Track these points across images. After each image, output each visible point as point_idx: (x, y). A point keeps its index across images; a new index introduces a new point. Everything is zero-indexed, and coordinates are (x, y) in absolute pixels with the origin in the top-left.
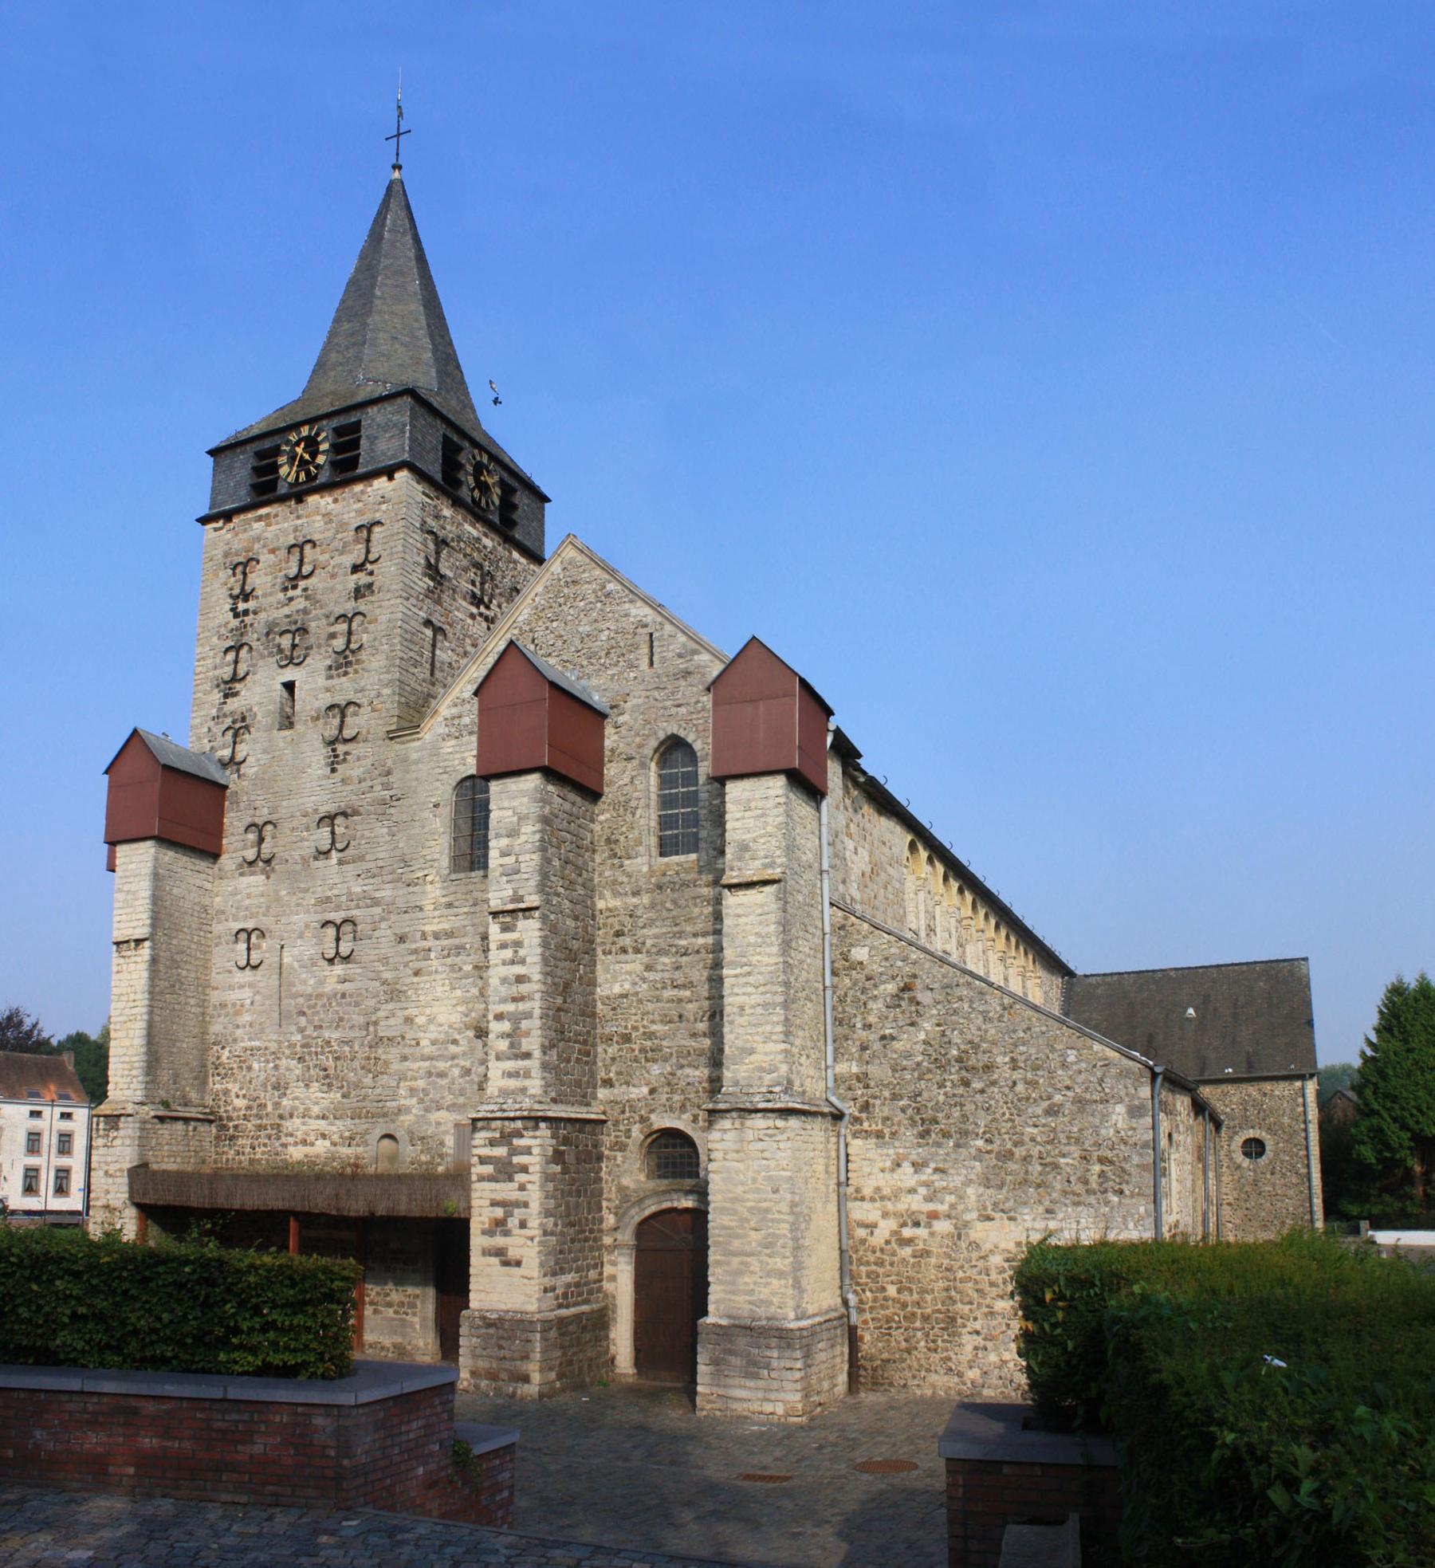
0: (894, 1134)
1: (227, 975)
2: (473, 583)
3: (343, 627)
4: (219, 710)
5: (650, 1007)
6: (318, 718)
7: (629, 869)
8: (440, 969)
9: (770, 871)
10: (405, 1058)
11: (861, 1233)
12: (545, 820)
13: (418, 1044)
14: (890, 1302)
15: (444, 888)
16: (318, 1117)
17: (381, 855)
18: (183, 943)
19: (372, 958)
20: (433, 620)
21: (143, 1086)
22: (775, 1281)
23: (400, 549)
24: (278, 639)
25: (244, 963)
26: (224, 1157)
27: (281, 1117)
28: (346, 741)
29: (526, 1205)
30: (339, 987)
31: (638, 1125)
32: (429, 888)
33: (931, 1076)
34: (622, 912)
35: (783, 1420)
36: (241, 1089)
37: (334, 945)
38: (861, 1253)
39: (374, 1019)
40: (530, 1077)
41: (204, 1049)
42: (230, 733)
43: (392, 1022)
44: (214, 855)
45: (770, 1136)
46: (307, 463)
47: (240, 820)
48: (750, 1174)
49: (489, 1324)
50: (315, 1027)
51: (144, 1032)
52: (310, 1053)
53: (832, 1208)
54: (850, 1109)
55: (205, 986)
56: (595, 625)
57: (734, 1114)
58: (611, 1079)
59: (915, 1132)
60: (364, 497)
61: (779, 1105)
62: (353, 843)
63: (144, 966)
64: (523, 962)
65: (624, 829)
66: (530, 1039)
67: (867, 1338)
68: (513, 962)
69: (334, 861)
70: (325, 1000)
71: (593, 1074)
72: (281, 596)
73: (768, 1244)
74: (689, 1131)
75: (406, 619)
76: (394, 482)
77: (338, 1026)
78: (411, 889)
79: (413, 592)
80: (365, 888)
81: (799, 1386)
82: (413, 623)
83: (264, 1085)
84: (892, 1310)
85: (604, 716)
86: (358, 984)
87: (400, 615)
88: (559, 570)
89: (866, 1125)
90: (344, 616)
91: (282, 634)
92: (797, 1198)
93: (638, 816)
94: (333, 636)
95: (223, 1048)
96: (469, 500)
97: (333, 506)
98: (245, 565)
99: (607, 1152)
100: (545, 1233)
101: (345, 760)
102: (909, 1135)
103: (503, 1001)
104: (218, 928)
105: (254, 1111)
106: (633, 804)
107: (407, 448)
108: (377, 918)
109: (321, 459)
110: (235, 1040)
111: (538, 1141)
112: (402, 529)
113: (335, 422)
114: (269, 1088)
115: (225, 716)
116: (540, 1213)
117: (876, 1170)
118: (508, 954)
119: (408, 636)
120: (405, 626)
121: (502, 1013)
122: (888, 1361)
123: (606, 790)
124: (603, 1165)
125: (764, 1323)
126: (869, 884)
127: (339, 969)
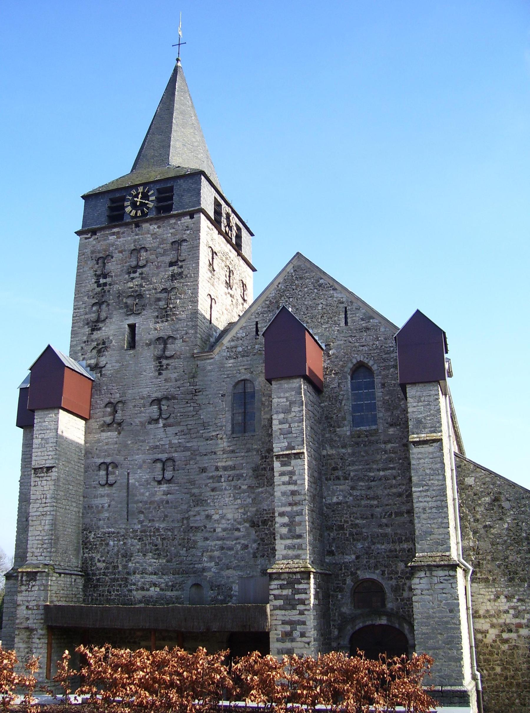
5: (355, 509)
10: (206, 539)
16: (151, 574)
27: (128, 573)
29: (304, 623)
30: (164, 497)
36: (101, 557)
39: (187, 516)
50: (149, 520)
52: (146, 536)
62: (172, 415)
68: (289, 483)
69: (161, 425)
80: (180, 441)
95: (90, 532)
98: (104, 258)
114: (120, 556)
115: (92, 341)
118: (286, 478)
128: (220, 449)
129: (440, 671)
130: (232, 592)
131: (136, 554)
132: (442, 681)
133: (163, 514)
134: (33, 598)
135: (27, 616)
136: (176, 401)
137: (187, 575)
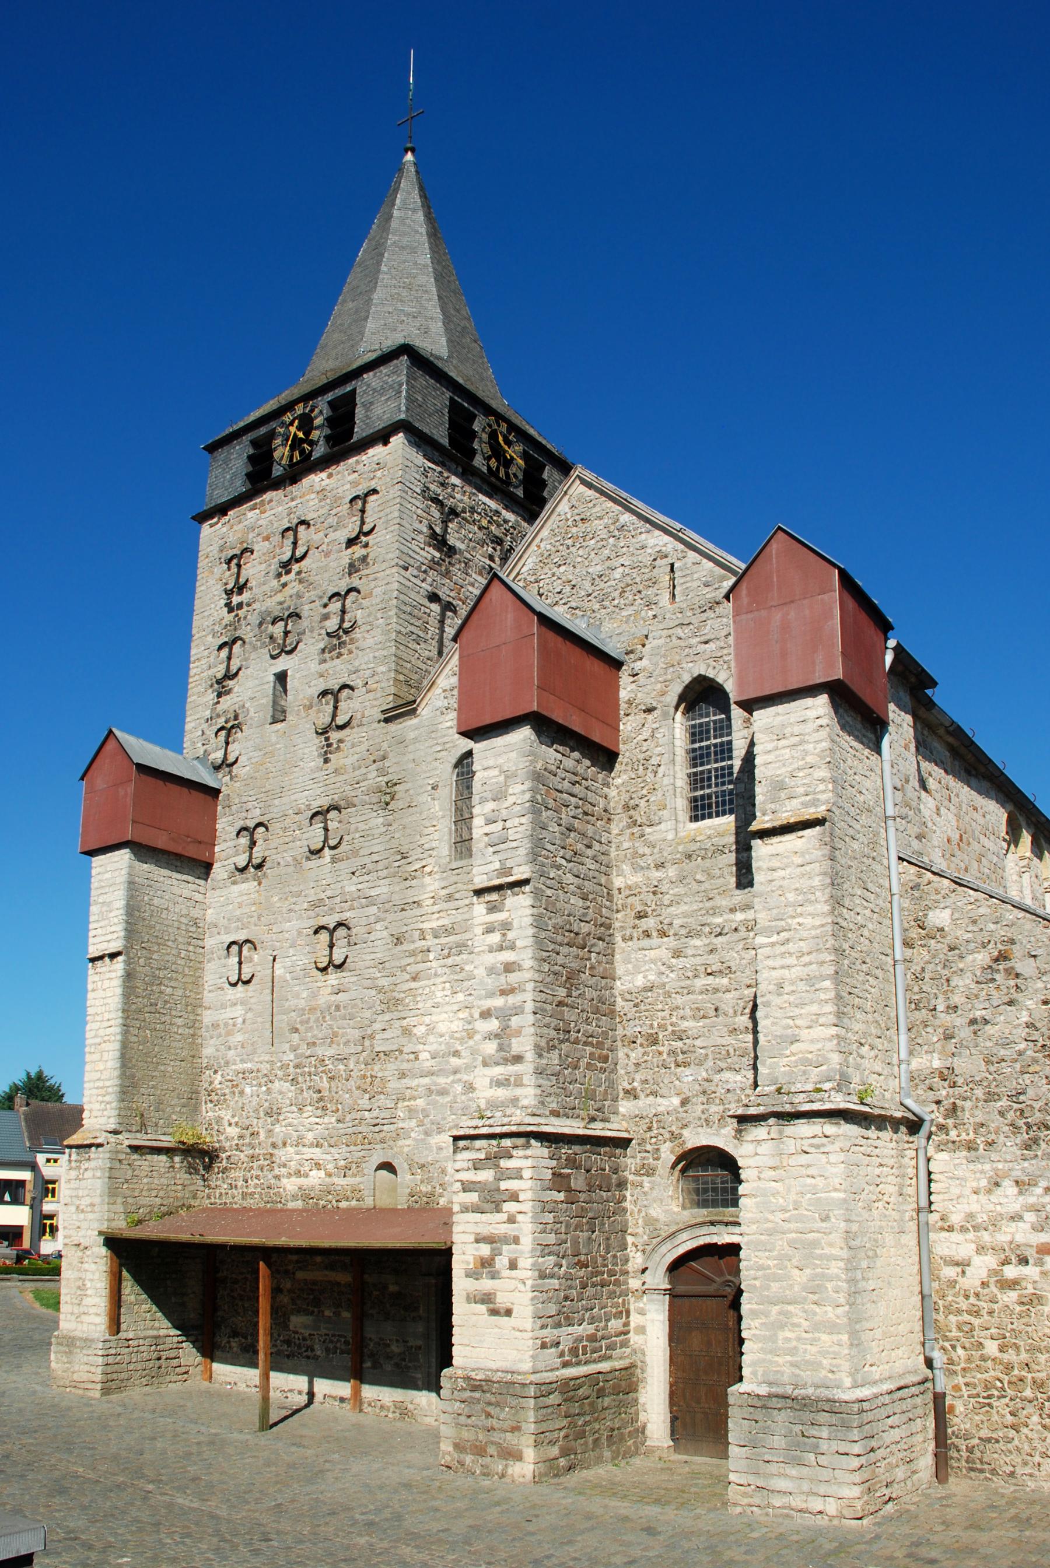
0: (990, 1144)
1: (220, 992)
2: (491, 558)
3: (336, 606)
4: (213, 710)
5: (679, 1000)
6: (311, 707)
7: (651, 838)
8: (440, 971)
9: (812, 810)
10: (403, 1075)
11: (950, 1272)
12: (537, 777)
13: (417, 1058)
14: (989, 1363)
15: (443, 879)
16: (311, 1145)
17: (375, 849)
18: (167, 958)
19: (368, 963)
20: (440, 594)
21: (117, 1112)
22: (824, 1337)
23: (396, 514)
24: (271, 629)
25: (236, 978)
26: (218, 1191)
27: (274, 1146)
28: (341, 728)
29: (516, 1240)
30: (333, 998)
31: (668, 1144)
32: (427, 880)
33: (1037, 1068)
34: (644, 889)
35: (836, 1522)
36: (233, 1116)
37: (327, 953)
38: (950, 1298)
39: (369, 1032)
40: (521, 1085)
41: (195, 1076)
42: (223, 733)
43: (387, 1034)
44: (203, 868)
45: (818, 1147)
46: (302, 441)
47: (232, 824)
48: (793, 1197)
49: (475, 1386)
50: (308, 1044)
51: (118, 1054)
52: (303, 1074)
53: (910, 1240)
54: (932, 1114)
55: (195, 1006)
56: (608, 563)
57: (772, 1121)
58: (634, 1089)
59: (1018, 1141)
60: (360, 467)
61: (828, 1106)
62: (346, 838)
63: (117, 982)
64: (512, 947)
65: (645, 792)
66: (520, 1039)
67: (960, 1408)
68: (501, 948)
69: (328, 859)
70: (319, 1013)
71: (612, 1084)
72: (275, 583)
73: (815, 1288)
74: (730, 1149)
75: (405, 590)
76: (390, 445)
77: (332, 1042)
78: (408, 883)
79: (412, 562)
80: (360, 886)
81: (857, 1477)
82: (413, 595)
83: (256, 1111)
84: (992, 1373)
85: (617, 664)
86: (352, 994)
87: (396, 585)
88: (567, 510)
89: (953, 1133)
90: (337, 594)
91: (273, 623)
92: (855, 1227)
93: (660, 774)
94: (326, 617)
95: (216, 1072)
96: (485, 469)
97: (327, 481)
98: (239, 557)
99: (631, 1177)
100: (543, 1276)
101: (338, 748)
102: (1010, 1146)
103: (490, 995)
104: (209, 942)
105: (247, 1141)
106: (654, 761)
107: (404, 408)
108: (372, 919)
109: (315, 435)
110: (227, 1063)
111: (529, 1162)
112: (399, 493)
113: (330, 396)
114: (262, 1114)
115: (218, 716)
116: (533, 1250)
117: (967, 1191)
118: (495, 938)
119: (408, 609)
120: (402, 596)
121: (489, 1010)
122: (989, 1440)
123: (622, 748)
124: (628, 1194)
125: (810, 1391)
126: (958, 853)
127: (333, 978)
128: (427, 896)
129: (793, 1352)
130: (447, 1178)
131: (287, 1109)
132: (798, 1376)
133: (330, 1031)
134: (86, 1192)
135: (78, 1224)
136: (354, 809)
137: (369, 1147)
